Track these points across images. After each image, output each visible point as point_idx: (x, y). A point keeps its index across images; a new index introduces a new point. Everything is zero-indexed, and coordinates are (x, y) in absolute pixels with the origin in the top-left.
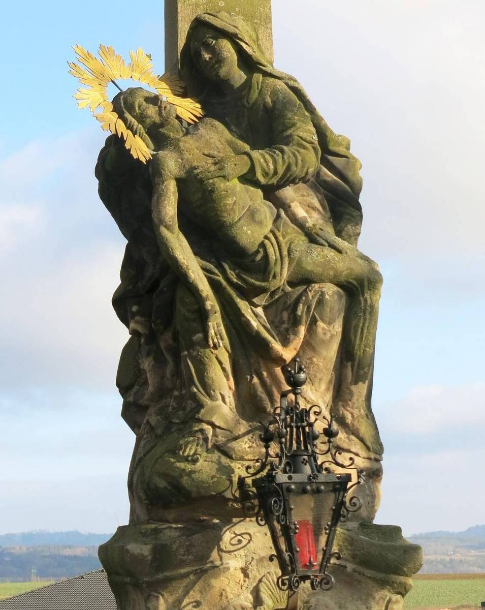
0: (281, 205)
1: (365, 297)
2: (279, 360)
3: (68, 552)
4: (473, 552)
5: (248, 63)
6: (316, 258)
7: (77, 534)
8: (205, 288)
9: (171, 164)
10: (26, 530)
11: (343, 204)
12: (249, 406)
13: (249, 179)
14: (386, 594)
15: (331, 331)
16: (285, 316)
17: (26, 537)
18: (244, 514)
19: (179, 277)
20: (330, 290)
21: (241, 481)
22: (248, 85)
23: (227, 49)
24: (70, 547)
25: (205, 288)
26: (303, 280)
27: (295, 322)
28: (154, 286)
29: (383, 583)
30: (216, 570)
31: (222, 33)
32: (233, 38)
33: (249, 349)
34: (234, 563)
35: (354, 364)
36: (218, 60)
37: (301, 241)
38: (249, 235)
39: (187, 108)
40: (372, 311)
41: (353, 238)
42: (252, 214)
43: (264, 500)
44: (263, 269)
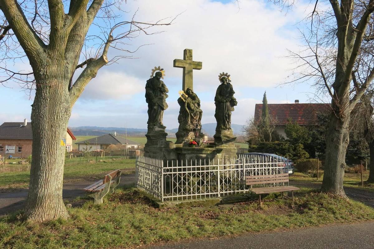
0: (195, 105)
1: (4, 36)
2: (194, 119)
3: (94, 130)
4: (173, 134)
5: (192, 92)
6: (198, 110)
7: (96, 127)
8: (189, 112)
9: (187, 102)
10: (86, 126)
11: (199, 105)
12: (192, 122)
13: (193, 103)
14: (202, 138)
15: (198, 116)
16: (195, 115)
17: (86, 127)
18: (191, 131)
19: (187, 111)
20: (198, 113)
21: (191, 129)
22: (192, 94)
23: (191, 91)
24: (94, 130)
25: (189, 112)
26: (196, 112)
27: (196, 115)
28: (183, 112)
29: (201, 137)
30: (188, 136)
31: (190, 90)
32: (191, 90)
33: (192, 118)
34: (190, 135)
35: (200, 119)
36: (190, 92)
37: (196, 109)
38: (193, 108)
39: (187, 96)
40: (202, 115)
41: (200, 108)
42: (193, 106)
43: (194, 130)
44: (194, 111)
